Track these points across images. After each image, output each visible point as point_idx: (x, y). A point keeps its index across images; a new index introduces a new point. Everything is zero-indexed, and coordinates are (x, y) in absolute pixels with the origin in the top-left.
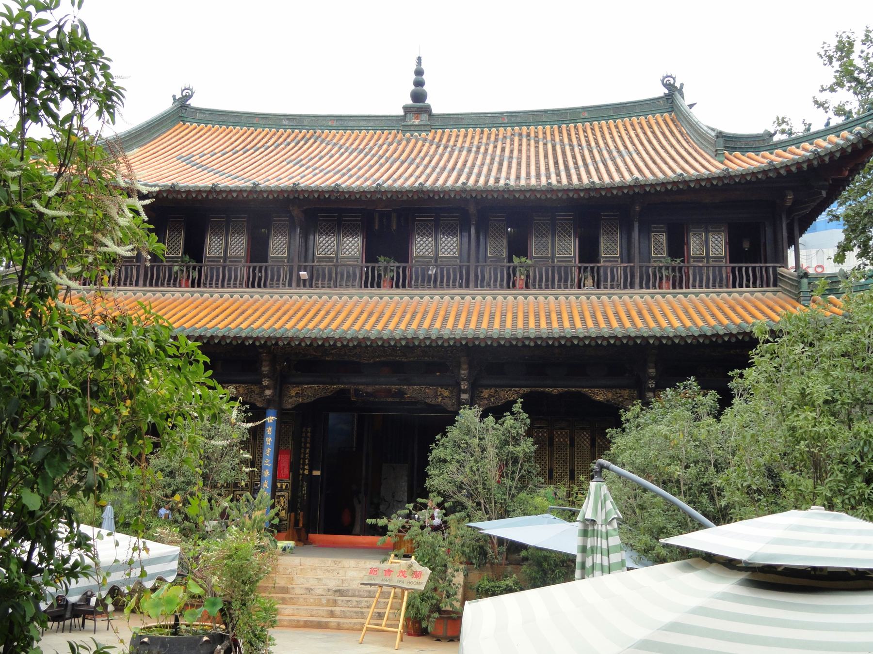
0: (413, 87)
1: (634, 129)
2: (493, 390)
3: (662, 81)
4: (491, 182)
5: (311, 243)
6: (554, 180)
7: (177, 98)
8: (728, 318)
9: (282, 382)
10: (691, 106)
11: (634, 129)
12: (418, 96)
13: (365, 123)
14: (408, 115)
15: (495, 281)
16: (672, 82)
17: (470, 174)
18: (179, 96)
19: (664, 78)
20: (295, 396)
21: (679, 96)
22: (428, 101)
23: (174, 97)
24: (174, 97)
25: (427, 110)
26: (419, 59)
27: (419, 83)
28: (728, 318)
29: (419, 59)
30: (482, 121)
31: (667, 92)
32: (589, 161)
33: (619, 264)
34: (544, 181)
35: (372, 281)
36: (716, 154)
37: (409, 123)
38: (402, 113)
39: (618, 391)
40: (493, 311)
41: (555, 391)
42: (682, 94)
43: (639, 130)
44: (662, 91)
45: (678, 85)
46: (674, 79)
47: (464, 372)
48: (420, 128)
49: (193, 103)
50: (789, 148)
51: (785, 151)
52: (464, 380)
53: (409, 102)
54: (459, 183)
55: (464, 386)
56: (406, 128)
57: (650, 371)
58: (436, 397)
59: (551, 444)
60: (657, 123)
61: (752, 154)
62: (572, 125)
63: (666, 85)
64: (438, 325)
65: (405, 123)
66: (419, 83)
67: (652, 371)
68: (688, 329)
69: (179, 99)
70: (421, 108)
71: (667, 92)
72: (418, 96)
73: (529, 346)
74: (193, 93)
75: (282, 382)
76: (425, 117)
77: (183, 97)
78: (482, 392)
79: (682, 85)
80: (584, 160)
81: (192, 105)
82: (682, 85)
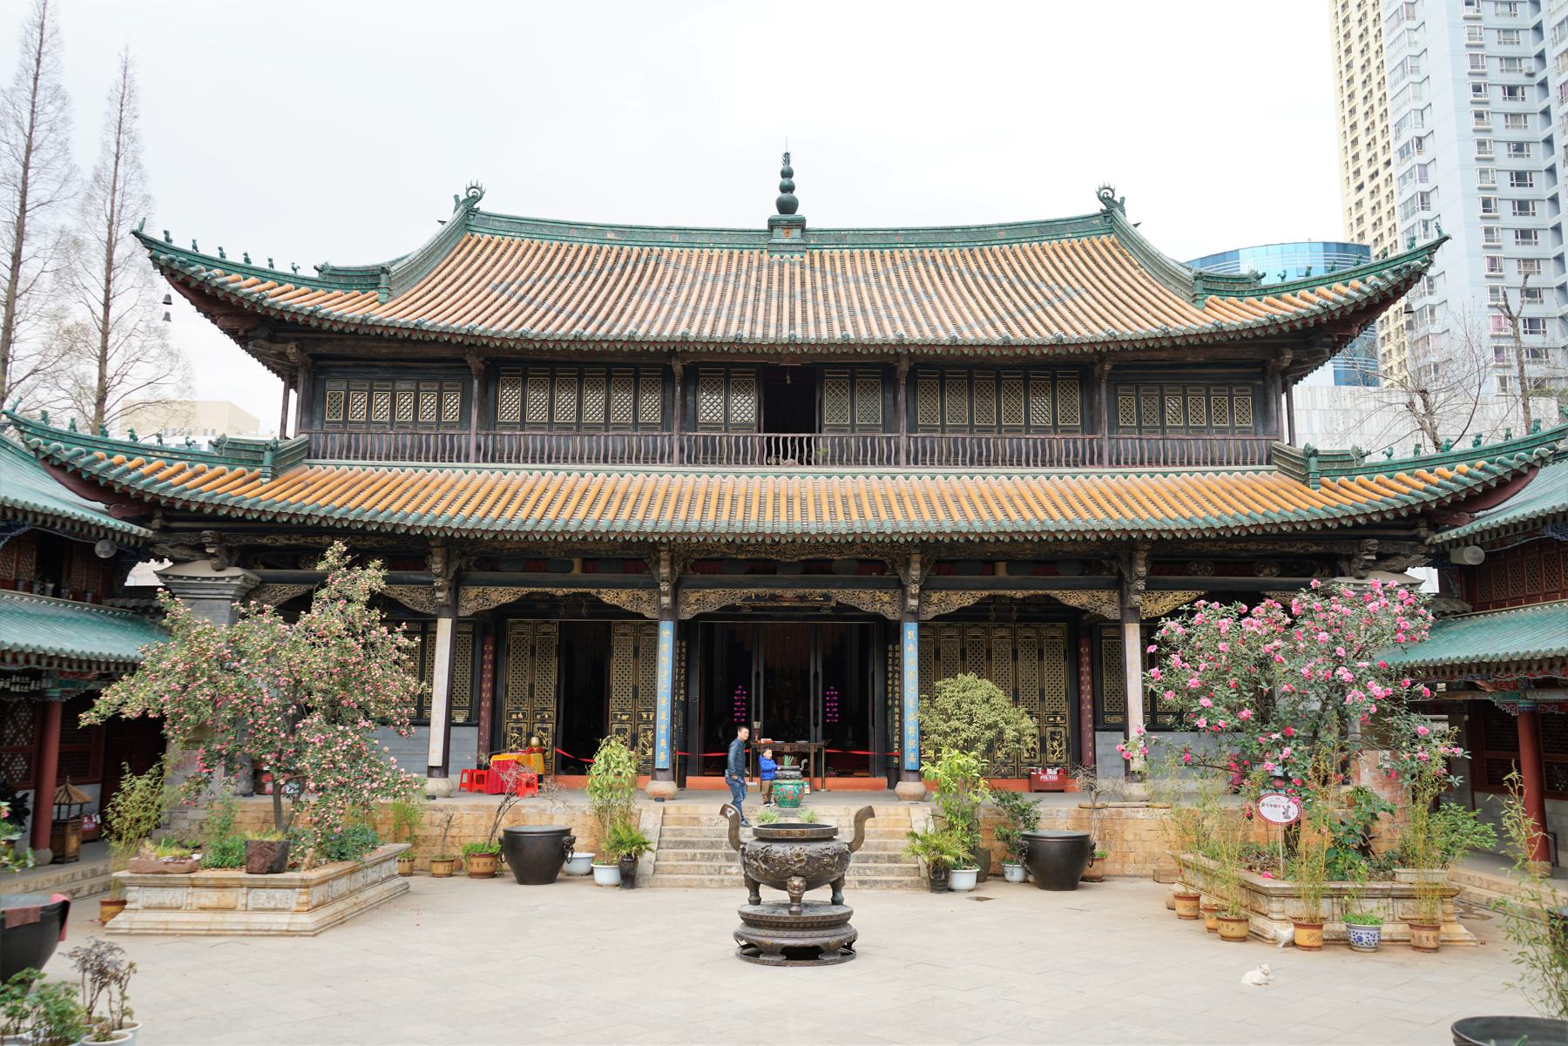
0: (779, 194)
1: (1006, 258)
2: (944, 593)
3: (1098, 194)
4: (772, 333)
5: (690, 405)
6: (799, 333)
7: (461, 199)
8: (991, 513)
9: (458, 584)
10: (1136, 225)
11: (1006, 258)
12: (787, 206)
13: (718, 239)
14: (776, 231)
15: (865, 455)
16: (1110, 195)
17: (741, 322)
18: (463, 197)
19: (1101, 190)
20: (475, 600)
21: (1121, 214)
22: (799, 212)
23: (456, 197)
24: (456, 197)
25: (800, 224)
26: (787, 155)
27: (787, 189)
28: (991, 513)
29: (787, 155)
30: (871, 240)
31: (1104, 208)
32: (880, 304)
33: (1079, 436)
34: (785, 334)
35: (773, 453)
36: (1194, 300)
37: (777, 241)
38: (765, 226)
39: (1095, 592)
40: (883, 492)
41: (1019, 594)
42: (1123, 211)
43: (932, 268)
44: (1097, 207)
45: (1117, 199)
46: (1113, 191)
47: (664, 571)
48: (789, 248)
49: (482, 206)
50: (1300, 292)
51: (1312, 292)
52: (914, 582)
53: (775, 212)
54: (679, 333)
55: (665, 587)
56: (773, 248)
57: (1140, 569)
58: (873, 602)
59: (937, 657)
60: (1014, 254)
61: (1253, 300)
62: (887, 252)
63: (1102, 199)
64: (697, 516)
65: (773, 241)
66: (787, 189)
67: (1142, 570)
68: (999, 524)
69: (464, 201)
70: (789, 221)
71: (1104, 208)
72: (787, 206)
73: (1255, 534)
74: (482, 193)
75: (458, 584)
76: (797, 232)
77: (469, 198)
78: (929, 596)
79: (1123, 199)
80: (873, 303)
81: (482, 209)
82: (1123, 199)
